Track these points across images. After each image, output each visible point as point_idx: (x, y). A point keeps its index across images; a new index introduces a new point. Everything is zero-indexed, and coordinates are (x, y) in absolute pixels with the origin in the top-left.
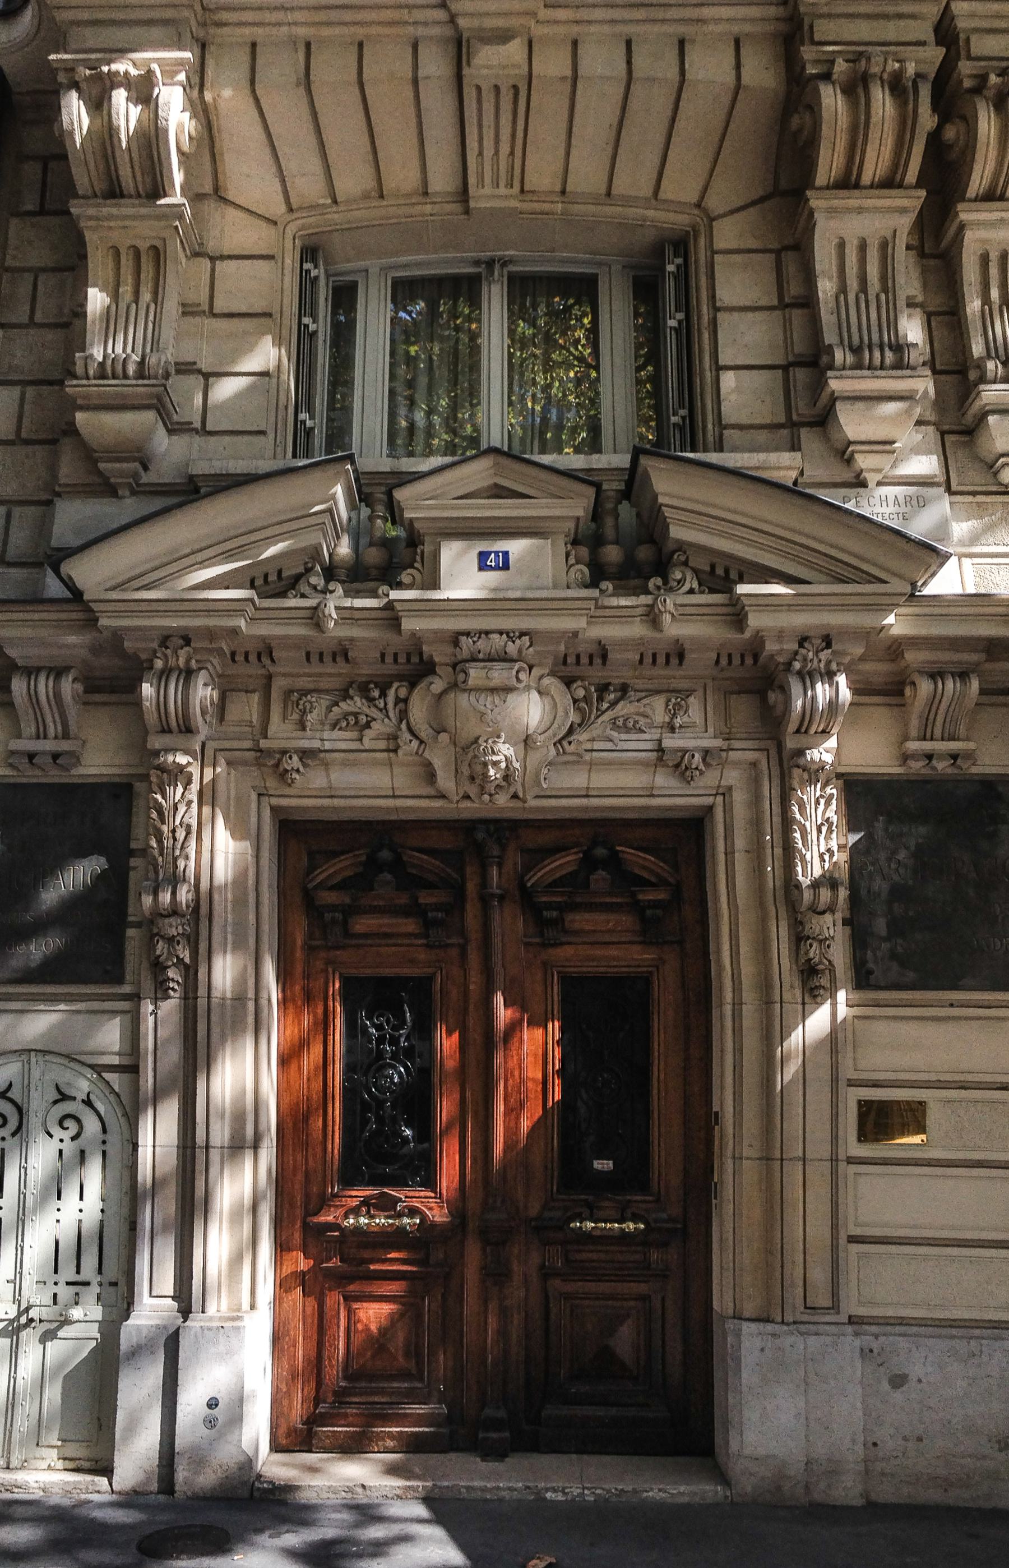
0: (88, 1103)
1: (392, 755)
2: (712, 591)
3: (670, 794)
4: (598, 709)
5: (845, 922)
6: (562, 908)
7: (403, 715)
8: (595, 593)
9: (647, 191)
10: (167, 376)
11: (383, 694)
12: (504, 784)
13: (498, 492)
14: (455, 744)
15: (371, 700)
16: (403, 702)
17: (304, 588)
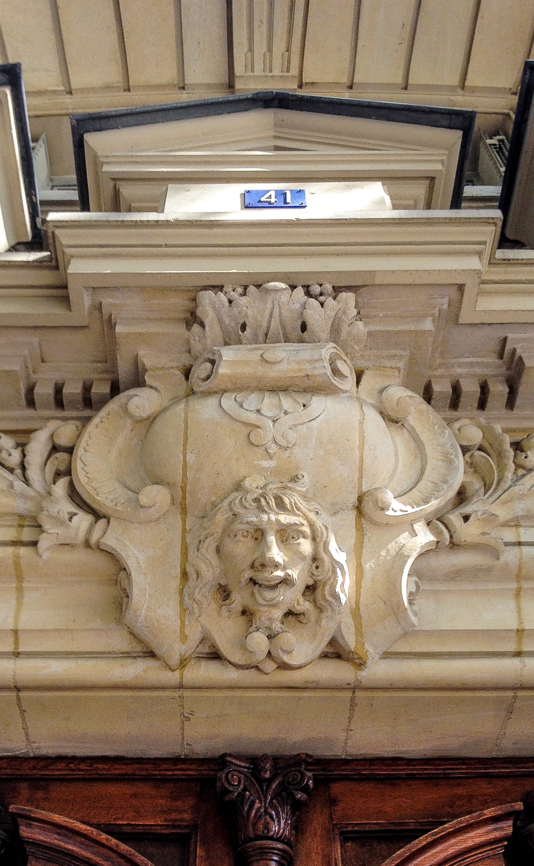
1: (23, 551)
4: (518, 466)
9: (455, 81)
12: (305, 606)
14: (184, 511)
16: (62, 451)
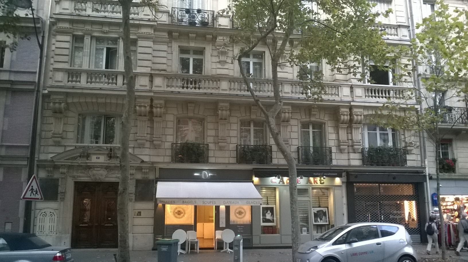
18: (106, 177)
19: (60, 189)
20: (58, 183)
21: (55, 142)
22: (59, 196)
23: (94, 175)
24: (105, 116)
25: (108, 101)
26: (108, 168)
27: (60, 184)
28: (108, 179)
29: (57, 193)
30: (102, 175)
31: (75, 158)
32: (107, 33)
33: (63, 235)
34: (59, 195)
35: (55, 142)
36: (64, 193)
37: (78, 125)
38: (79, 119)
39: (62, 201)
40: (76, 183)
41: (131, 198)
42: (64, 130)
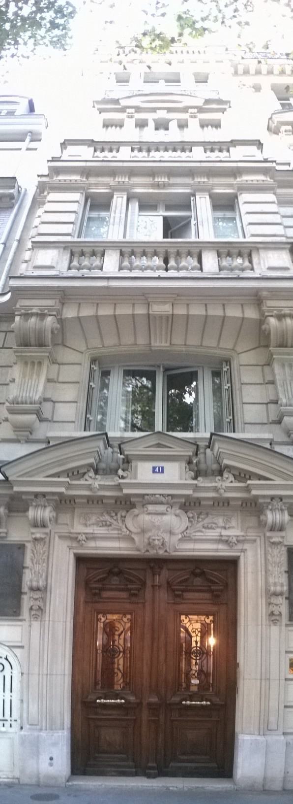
0: (6, 659)
2: (239, 481)
3: (223, 551)
5: (286, 598)
6: (183, 591)
7: (123, 521)
8: (195, 482)
10: (40, 403)
11: (116, 515)
13: (159, 445)
15: (112, 517)
17: (86, 477)
18: (185, 539)
19: (28, 578)
20: (23, 562)
21: (17, 428)
22: (26, 602)
23: (143, 531)
24: (166, 370)
25: (180, 311)
26: (189, 505)
27: (28, 562)
28: (190, 546)
29: (17, 593)
30: (171, 533)
31: (76, 473)
32: (165, 186)
33: (43, 734)
34: (25, 598)
35: (17, 428)
36: (41, 590)
37: (90, 388)
38: (92, 371)
39: (36, 617)
40: (81, 561)
41: (276, 610)
42: (48, 396)
